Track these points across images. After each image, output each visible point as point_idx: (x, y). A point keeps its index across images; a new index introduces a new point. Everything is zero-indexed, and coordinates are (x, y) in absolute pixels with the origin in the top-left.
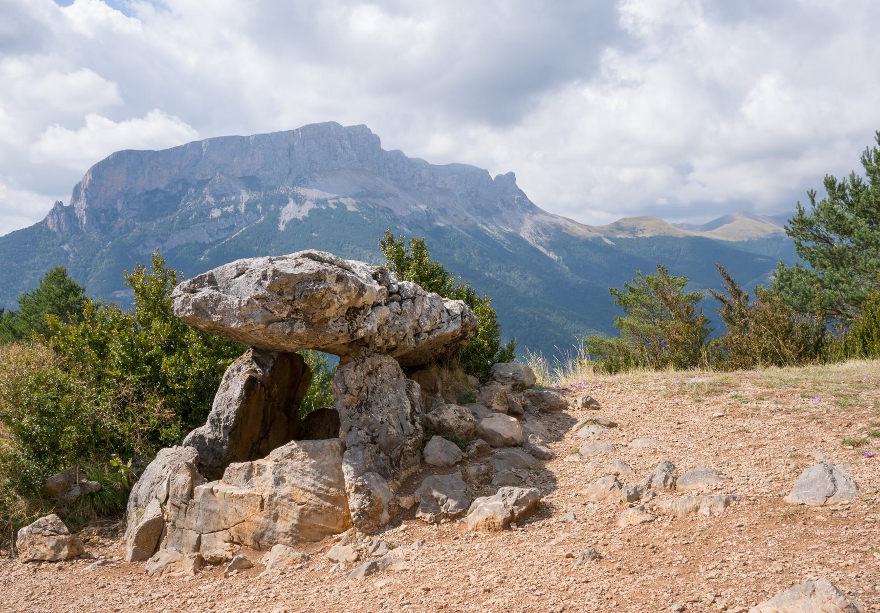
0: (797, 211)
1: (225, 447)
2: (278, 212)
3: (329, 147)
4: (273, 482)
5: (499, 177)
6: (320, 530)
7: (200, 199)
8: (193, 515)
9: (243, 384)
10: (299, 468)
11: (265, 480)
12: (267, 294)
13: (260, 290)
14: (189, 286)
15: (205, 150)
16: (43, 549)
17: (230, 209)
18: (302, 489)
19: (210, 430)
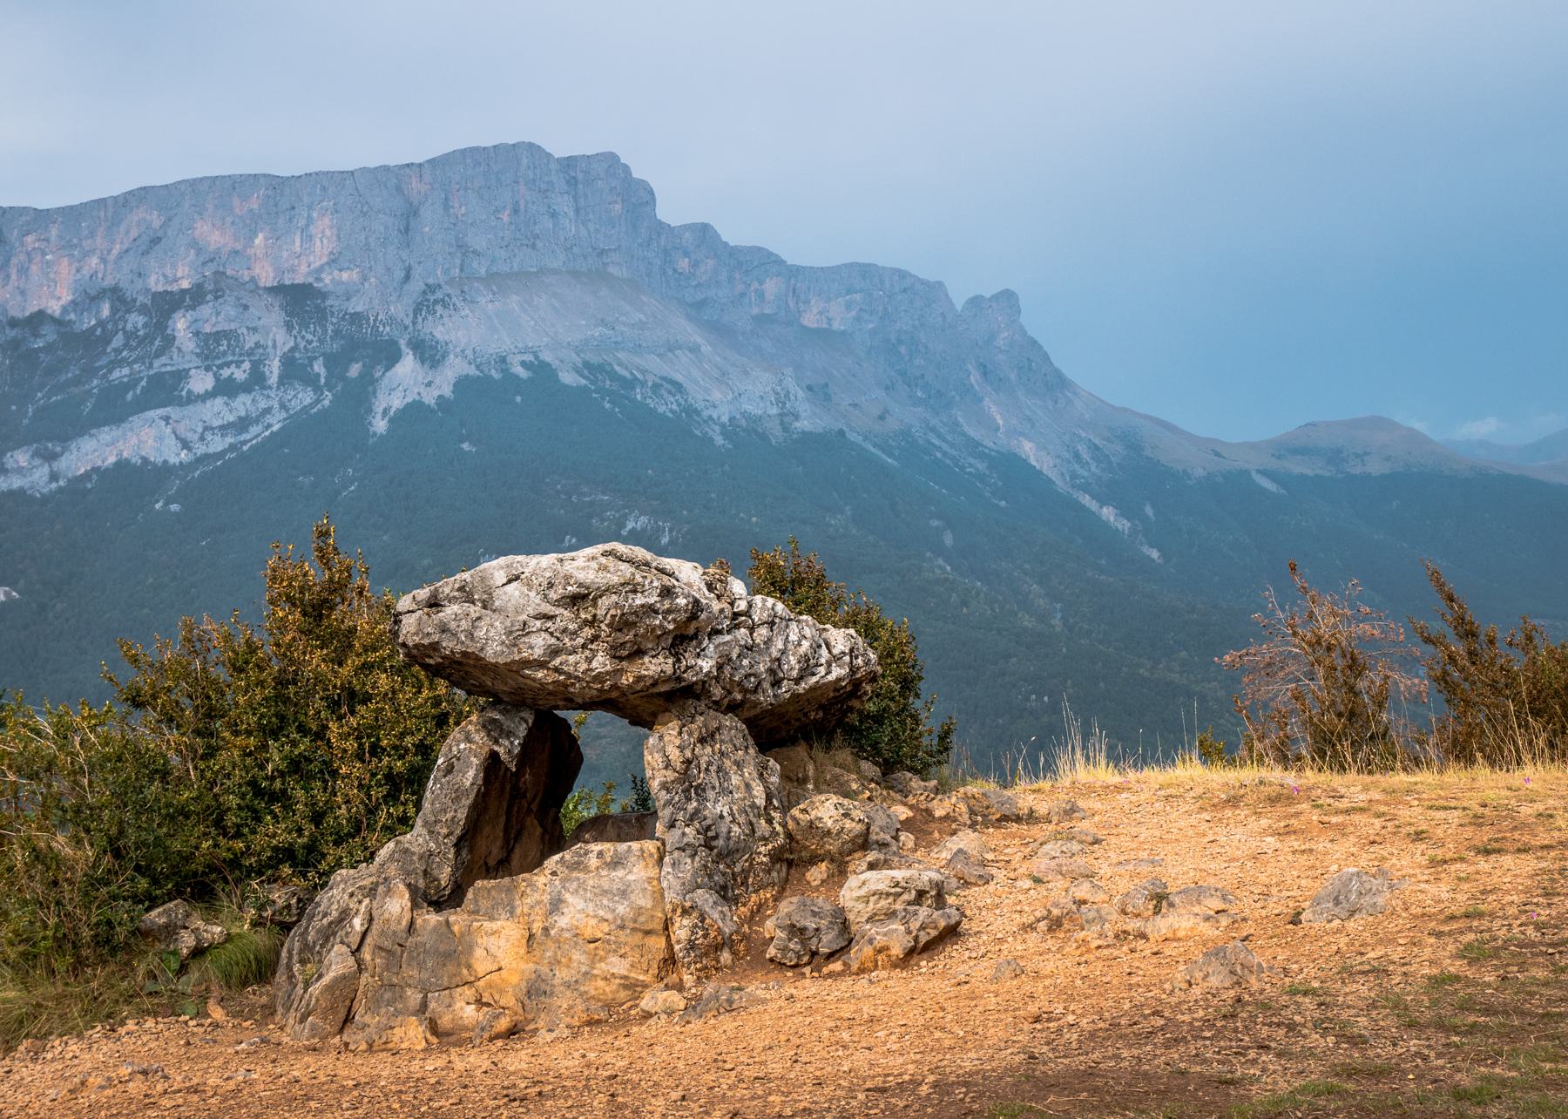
5: (976, 302)
6: (622, 981)
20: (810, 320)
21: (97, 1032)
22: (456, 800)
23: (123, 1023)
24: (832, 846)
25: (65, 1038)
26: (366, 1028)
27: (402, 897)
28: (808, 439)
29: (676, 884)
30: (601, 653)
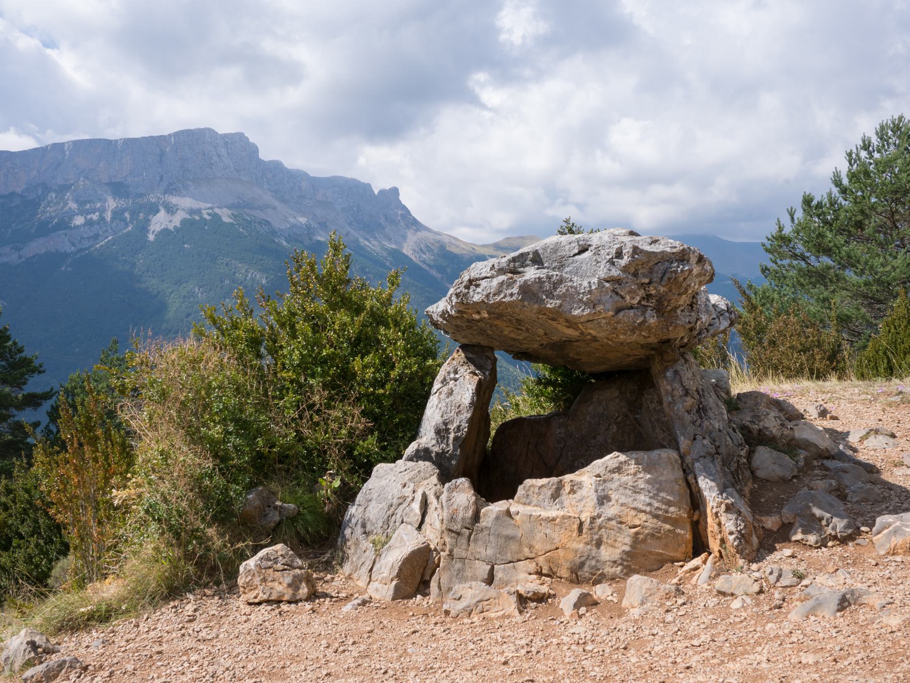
0: (777, 227)
1: (453, 462)
2: (147, 221)
3: (204, 154)
4: (595, 500)
5: (382, 192)
6: (657, 557)
7: (61, 204)
8: (480, 543)
9: (474, 388)
10: (630, 484)
11: (581, 500)
12: (622, 275)
13: (613, 270)
14: (508, 266)
15: (67, 153)
16: (280, 588)
17: (95, 217)
18: (635, 509)
19: (434, 442)
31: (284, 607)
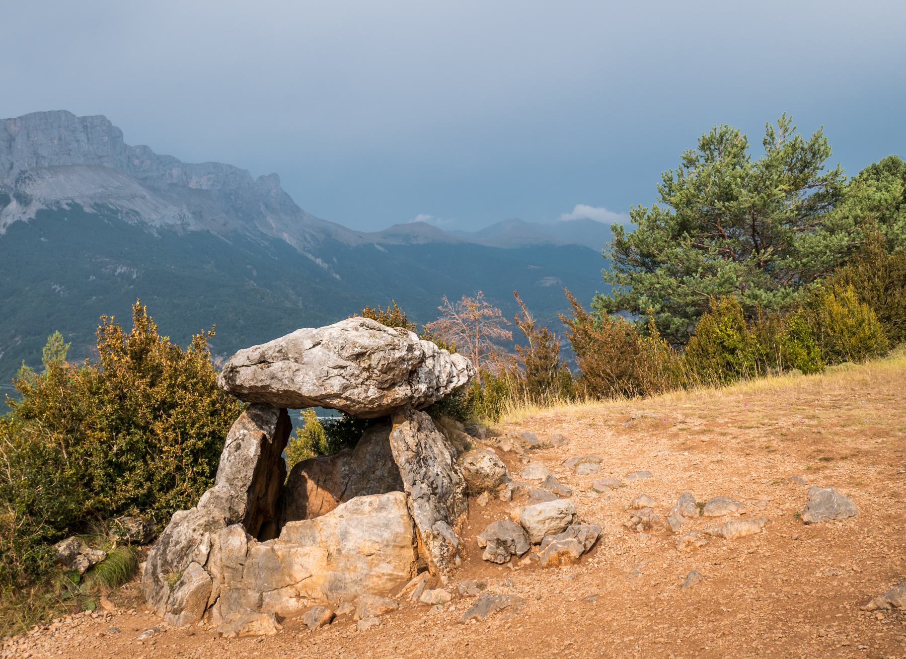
20: (193, 185)
21: (36, 632)
22: (246, 465)
23: (51, 622)
24: (489, 483)
25: (15, 638)
26: (232, 622)
27: (240, 535)
28: (193, 233)
29: (425, 520)
30: (372, 387)
31: (410, 553)
